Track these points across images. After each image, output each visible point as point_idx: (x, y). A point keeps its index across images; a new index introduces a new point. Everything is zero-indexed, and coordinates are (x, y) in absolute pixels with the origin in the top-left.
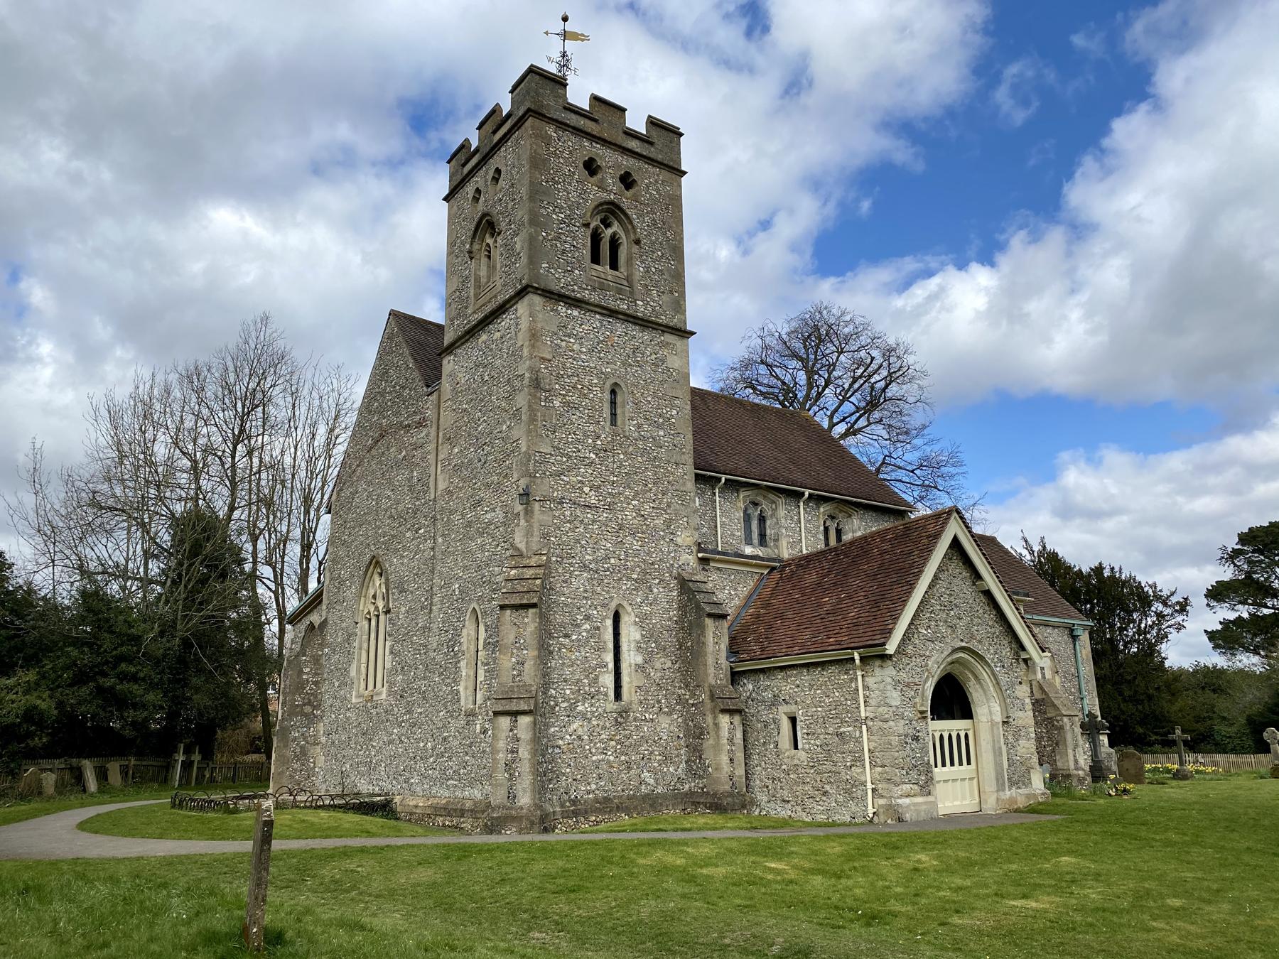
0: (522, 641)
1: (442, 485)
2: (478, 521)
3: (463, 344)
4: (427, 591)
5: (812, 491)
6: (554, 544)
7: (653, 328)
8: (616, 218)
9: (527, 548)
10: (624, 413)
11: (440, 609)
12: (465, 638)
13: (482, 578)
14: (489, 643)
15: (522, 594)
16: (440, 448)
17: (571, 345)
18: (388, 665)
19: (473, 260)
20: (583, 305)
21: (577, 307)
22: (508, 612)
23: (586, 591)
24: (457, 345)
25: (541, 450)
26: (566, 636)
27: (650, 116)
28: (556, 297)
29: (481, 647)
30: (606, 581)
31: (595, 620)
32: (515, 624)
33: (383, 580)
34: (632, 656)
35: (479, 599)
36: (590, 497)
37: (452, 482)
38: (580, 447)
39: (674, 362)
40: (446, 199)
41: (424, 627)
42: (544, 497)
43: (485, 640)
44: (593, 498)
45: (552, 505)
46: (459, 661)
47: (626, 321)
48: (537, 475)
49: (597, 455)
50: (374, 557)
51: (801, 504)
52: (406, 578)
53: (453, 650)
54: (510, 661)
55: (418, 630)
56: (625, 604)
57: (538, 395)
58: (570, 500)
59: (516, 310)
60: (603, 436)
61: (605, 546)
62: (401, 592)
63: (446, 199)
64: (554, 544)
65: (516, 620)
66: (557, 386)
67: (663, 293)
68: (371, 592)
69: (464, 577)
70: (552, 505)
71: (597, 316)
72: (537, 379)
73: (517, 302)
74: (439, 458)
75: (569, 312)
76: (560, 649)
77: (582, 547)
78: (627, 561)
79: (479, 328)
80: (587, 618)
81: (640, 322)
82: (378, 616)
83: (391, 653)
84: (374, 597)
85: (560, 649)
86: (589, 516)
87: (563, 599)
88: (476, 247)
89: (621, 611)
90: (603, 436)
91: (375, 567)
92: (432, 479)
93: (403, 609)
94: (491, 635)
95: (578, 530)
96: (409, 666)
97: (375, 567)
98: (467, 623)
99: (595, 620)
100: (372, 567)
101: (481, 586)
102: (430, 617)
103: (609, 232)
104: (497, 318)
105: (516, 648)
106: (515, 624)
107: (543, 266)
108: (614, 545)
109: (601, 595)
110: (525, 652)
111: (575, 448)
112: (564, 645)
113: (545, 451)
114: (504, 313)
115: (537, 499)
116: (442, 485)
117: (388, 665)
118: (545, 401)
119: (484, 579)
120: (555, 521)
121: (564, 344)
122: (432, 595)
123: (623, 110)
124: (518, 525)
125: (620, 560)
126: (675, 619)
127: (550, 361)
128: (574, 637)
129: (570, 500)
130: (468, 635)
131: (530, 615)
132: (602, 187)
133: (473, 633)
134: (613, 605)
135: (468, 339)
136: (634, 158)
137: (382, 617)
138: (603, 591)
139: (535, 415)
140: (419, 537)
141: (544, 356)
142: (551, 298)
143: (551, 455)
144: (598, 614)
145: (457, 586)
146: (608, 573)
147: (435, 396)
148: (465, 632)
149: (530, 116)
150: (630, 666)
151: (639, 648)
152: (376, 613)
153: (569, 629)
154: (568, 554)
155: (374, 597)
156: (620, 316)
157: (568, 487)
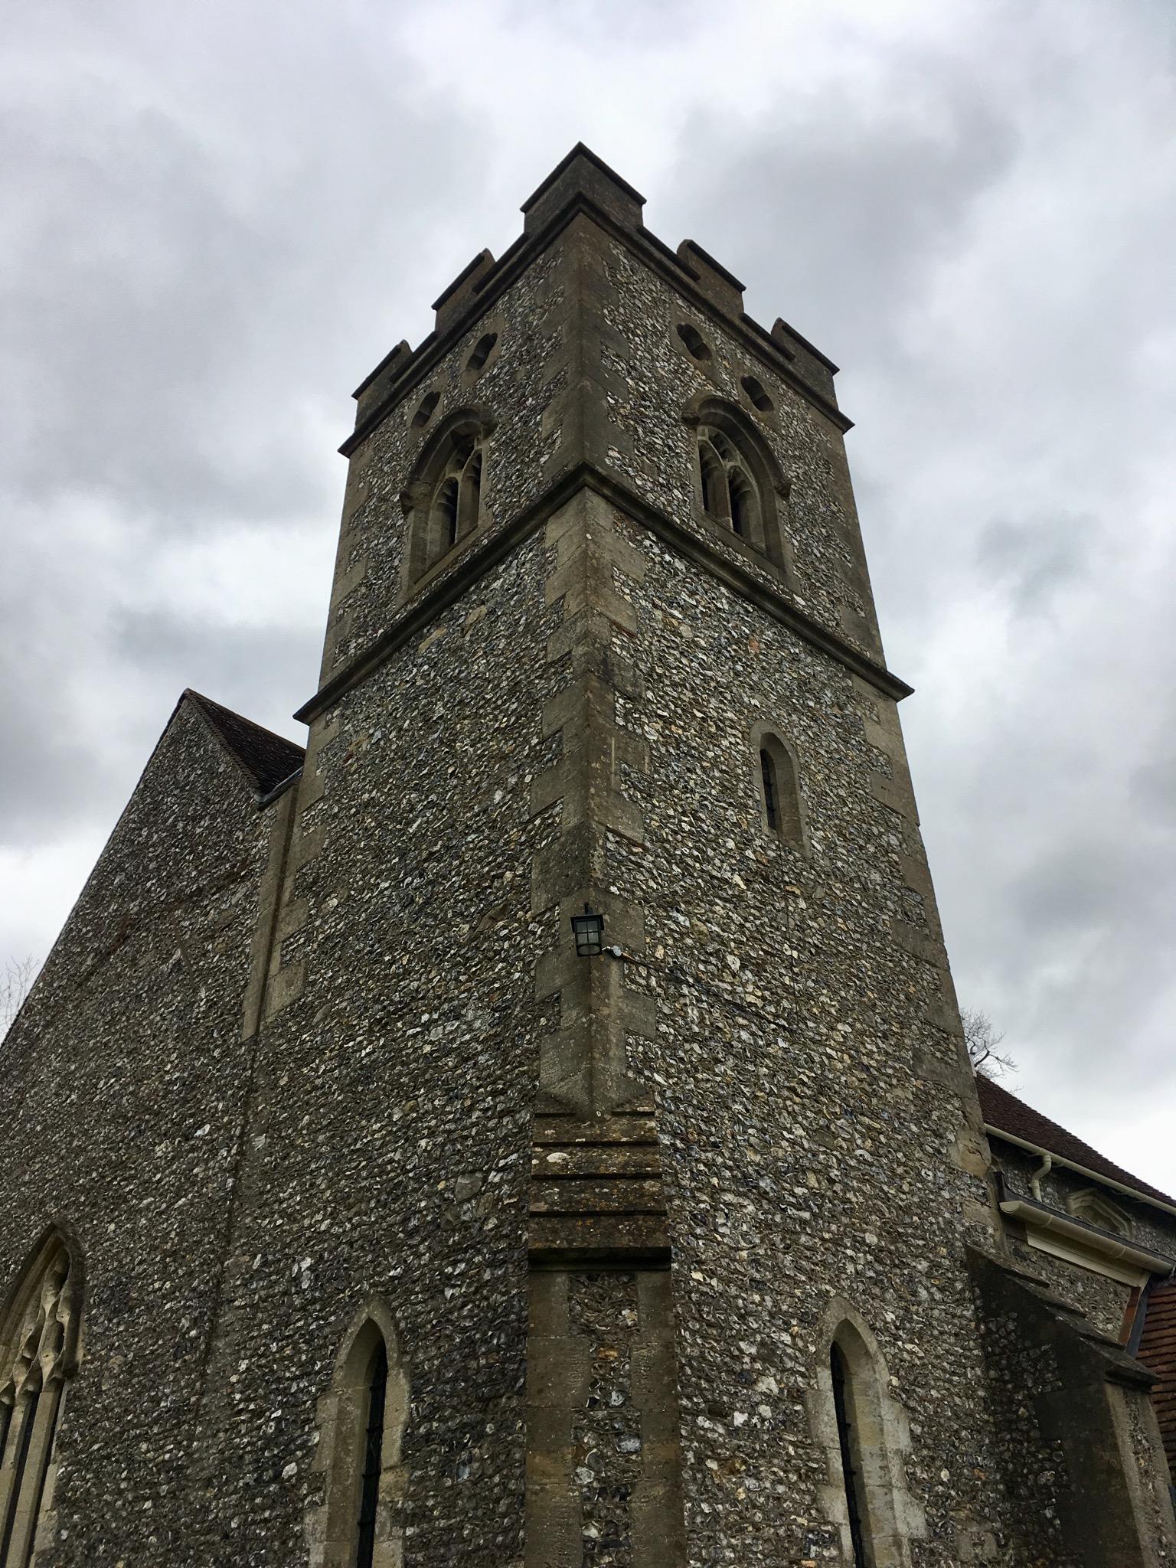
0: (616, 1399)
1: (280, 997)
2: (396, 1056)
3: (370, 674)
4: (201, 1295)
5: (1057, 1156)
6: (662, 1094)
7: (831, 656)
8: (736, 445)
9: (590, 1090)
10: (795, 806)
11: (242, 1344)
12: (330, 1428)
13: (406, 1220)
14: (428, 1438)
15: (605, 1222)
16: (283, 912)
17: (676, 623)
18: (44, 1540)
19: (412, 514)
20: (697, 555)
21: (682, 555)
22: (561, 1281)
23: (755, 1262)
24: (355, 679)
25: (620, 828)
26: (719, 1413)
27: (779, 320)
28: (641, 516)
29: (391, 1451)
30: (803, 1239)
31: (789, 1364)
32: (588, 1330)
33: (65, 1292)
34: (898, 1506)
35: (387, 1293)
36: (744, 985)
37: (313, 983)
38: (711, 853)
39: (874, 733)
40: (346, 449)
41: (177, 1411)
42: (633, 952)
43: (411, 1424)
44: (750, 988)
45: (653, 982)
46: (298, 1515)
47: (780, 621)
48: (613, 889)
49: (747, 882)
50: (52, 1228)
51: (1036, 1184)
52: (139, 1269)
53: (277, 1477)
54: (572, 1478)
55: (156, 1421)
56: (860, 1324)
57: (610, 697)
58: (698, 980)
59: (541, 539)
60: (758, 842)
61: (790, 1132)
62: (117, 1312)
63: (346, 449)
64: (662, 1094)
65: (591, 1316)
66: (650, 695)
67: (838, 599)
68: (27, 1330)
69: (335, 1230)
70: (653, 982)
71: (723, 589)
72: (604, 661)
73: (544, 522)
74: (280, 936)
75: (667, 558)
76: (700, 1459)
77: (735, 1120)
78: (847, 1188)
79: (424, 618)
80: (769, 1354)
81: (807, 632)
82: (33, 1398)
83: (60, 1499)
84: (33, 1344)
85: (700, 1459)
86: (744, 1035)
87: (697, 1276)
88: (419, 489)
89: (844, 1347)
90: (758, 842)
91: (48, 1260)
92: (251, 996)
93: (116, 1361)
94: (435, 1408)
95: (722, 1068)
96: (115, 1540)
97: (48, 1260)
98: (338, 1376)
99: (789, 1364)
100: (41, 1258)
101: (397, 1247)
102: (203, 1375)
103: (728, 465)
104: (476, 580)
105: (597, 1427)
106: (588, 1330)
107: (611, 453)
108: (812, 1133)
109: (797, 1283)
110: (631, 1444)
111: (698, 849)
112: (711, 1444)
113: (629, 833)
114: (501, 561)
115: (618, 952)
116: (280, 997)
117: (44, 1540)
118: (625, 717)
119: (414, 1222)
120: (663, 1028)
121: (658, 614)
122: (218, 1304)
123: (742, 288)
124: (552, 1030)
125: (832, 1181)
126: (981, 1393)
127: (631, 635)
128: (739, 1419)
129: (698, 980)
130: (341, 1416)
131: (642, 1297)
132: (712, 377)
133: (356, 1412)
134: (831, 1319)
135: (390, 656)
136: (764, 365)
137: (46, 1399)
138: (800, 1269)
139: (604, 741)
140: (193, 1149)
141: (618, 620)
142: (629, 516)
143: (646, 849)
144: (795, 1344)
145: (308, 1262)
146: (806, 1215)
147: (281, 805)
148: (329, 1407)
149: (580, 210)
150: (899, 1546)
151: (912, 1483)
152: (30, 1388)
153: (724, 1389)
154: (700, 1132)
155: (33, 1344)
156: (769, 606)
157: (689, 941)
